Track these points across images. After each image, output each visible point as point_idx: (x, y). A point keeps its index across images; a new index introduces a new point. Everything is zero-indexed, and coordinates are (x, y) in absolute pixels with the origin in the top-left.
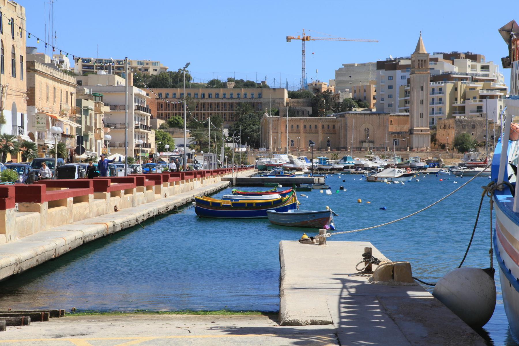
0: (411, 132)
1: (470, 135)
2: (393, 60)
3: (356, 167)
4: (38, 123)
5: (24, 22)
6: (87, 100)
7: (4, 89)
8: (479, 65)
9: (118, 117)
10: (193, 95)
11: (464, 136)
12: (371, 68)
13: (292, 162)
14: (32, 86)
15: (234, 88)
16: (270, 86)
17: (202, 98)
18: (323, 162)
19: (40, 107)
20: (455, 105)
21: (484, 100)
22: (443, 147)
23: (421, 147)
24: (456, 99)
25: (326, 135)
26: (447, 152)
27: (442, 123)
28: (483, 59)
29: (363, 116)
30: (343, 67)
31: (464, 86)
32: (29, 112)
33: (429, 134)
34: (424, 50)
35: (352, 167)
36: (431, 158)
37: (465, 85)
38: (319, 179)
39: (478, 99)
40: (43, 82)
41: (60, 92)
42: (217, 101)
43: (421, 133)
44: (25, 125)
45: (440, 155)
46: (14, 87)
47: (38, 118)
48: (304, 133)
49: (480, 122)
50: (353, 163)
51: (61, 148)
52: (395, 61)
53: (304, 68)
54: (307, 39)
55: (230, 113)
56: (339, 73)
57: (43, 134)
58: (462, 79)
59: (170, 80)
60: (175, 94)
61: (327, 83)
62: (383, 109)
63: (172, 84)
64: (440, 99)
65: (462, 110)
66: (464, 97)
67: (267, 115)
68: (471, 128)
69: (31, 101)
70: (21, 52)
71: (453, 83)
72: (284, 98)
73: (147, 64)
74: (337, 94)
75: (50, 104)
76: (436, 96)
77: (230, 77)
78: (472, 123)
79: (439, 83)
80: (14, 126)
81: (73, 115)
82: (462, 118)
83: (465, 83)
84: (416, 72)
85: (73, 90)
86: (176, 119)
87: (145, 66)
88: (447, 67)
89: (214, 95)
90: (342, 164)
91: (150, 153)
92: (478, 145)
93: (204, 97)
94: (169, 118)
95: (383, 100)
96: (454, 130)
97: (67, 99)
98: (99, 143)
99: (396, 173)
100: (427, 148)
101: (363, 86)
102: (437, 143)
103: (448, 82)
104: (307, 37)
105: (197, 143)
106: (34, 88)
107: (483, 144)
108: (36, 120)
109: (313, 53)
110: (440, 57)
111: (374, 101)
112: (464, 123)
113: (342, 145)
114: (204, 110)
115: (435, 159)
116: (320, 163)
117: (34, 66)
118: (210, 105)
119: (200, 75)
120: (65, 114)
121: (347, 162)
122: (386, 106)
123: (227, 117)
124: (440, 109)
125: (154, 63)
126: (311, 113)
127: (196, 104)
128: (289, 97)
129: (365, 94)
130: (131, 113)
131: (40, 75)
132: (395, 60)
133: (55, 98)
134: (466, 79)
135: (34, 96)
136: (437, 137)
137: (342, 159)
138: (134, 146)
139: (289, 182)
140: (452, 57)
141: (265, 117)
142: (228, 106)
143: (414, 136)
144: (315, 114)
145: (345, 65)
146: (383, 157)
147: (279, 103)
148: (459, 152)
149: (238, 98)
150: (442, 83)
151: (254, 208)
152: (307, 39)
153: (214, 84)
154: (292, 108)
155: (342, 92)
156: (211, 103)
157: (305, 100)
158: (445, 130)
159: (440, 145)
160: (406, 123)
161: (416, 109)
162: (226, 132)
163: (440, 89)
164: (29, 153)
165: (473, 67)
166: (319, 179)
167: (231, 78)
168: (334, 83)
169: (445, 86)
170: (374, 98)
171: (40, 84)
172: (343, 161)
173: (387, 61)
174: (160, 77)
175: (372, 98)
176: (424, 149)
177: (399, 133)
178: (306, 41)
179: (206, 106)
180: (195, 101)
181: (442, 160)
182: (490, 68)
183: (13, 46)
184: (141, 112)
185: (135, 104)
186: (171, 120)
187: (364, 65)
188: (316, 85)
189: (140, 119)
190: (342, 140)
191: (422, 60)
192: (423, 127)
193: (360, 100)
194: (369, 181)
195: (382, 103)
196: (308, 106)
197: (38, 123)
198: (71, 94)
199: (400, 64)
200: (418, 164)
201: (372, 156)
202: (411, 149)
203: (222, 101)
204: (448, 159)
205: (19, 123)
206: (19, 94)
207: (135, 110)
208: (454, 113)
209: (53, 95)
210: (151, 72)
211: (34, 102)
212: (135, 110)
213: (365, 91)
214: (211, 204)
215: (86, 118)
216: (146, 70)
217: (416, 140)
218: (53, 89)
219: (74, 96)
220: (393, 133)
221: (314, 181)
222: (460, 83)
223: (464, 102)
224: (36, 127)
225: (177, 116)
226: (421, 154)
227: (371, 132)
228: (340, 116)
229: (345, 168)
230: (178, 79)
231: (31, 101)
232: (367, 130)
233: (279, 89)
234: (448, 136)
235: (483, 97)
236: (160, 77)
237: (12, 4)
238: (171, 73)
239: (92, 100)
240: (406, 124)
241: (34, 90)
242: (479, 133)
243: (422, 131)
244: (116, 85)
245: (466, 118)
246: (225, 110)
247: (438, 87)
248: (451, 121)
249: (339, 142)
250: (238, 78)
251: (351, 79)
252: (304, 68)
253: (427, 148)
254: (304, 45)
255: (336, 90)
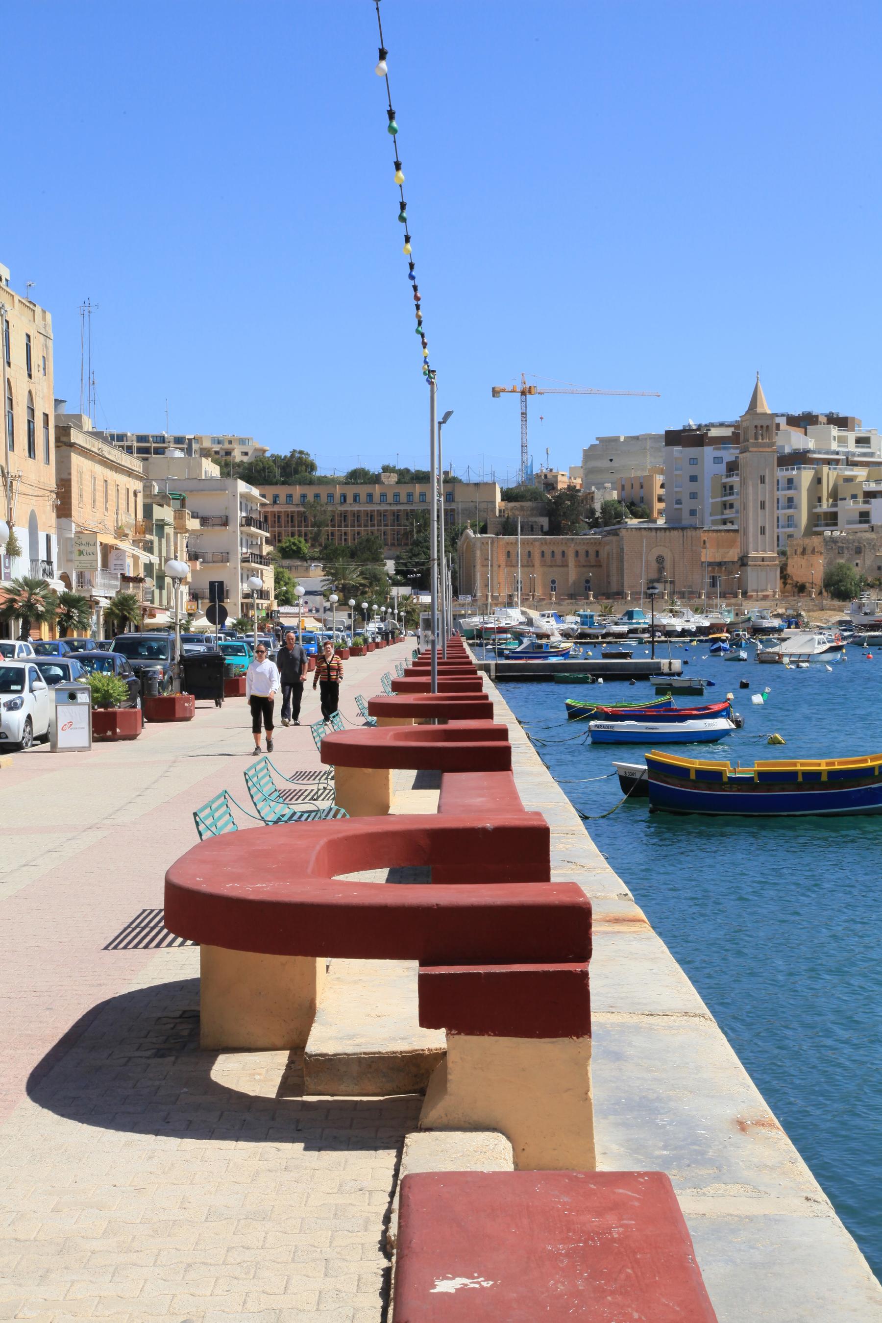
0: (743, 562)
1: (851, 566)
2: (694, 427)
3: (652, 629)
4: (81, 553)
5: (50, 344)
6: (162, 506)
7: (14, 482)
8: (851, 437)
9: (216, 539)
10: (324, 499)
11: (841, 567)
12: (649, 444)
13: (530, 622)
14: (65, 476)
15: (397, 483)
16: (464, 479)
17: (341, 504)
18: (586, 620)
19: (81, 521)
20: (818, 510)
21: (873, 501)
22: (801, 589)
23: (762, 591)
24: (820, 500)
25: (584, 569)
26: (813, 599)
27: (798, 545)
28: (859, 426)
29: (654, 533)
30: (598, 442)
31: (833, 475)
32: (60, 529)
33: (776, 565)
34: (766, 407)
35: (644, 631)
36: (784, 611)
37: (835, 473)
38: (670, 663)
39: (861, 499)
40: (84, 470)
41: (115, 489)
42: (369, 508)
43: (761, 563)
44: (54, 558)
45: (800, 604)
46: (32, 477)
47: (81, 544)
48: (576, 567)
49: (869, 541)
50: (645, 623)
51: (128, 606)
52: (699, 429)
53: (524, 446)
54: (530, 392)
55: (393, 530)
56: (590, 454)
57: (87, 576)
58: (828, 462)
59: (277, 471)
60: (290, 496)
61: (567, 474)
62: (680, 520)
63: (282, 479)
64: (790, 500)
65: (832, 519)
66: (835, 495)
67: (470, 532)
68: (853, 552)
69: (64, 510)
70: (44, 406)
71: (813, 468)
72: (495, 502)
73: (230, 442)
74: (589, 493)
75: (97, 515)
76: (783, 494)
77: (386, 463)
78: (856, 544)
79: (787, 470)
80: (34, 560)
81: (138, 537)
82: (836, 534)
83: (835, 469)
84: (751, 449)
85: (138, 485)
86: (294, 544)
87: (227, 446)
88: (796, 440)
89: (363, 498)
90: (624, 624)
91: (268, 608)
92: (868, 585)
93: (345, 501)
94: (280, 541)
95: (679, 502)
96: (823, 557)
97: (128, 504)
98: (182, 592)
99: (816, 645)
100: (775, 592)
101: (640, 477)
102: (789, 581)
103: (805, 468)
104: (530, 388)
105: (337, 587)
106: (69, 480)
107: (877, 583)
108: (77, 548)
109: (542, 418)
110: (782, 421)
111: (658, 506)
112: (840, 545)
113: (614, 588)
114: (346, 526)
115: (790, 612)
116: (583, 623)
117: (69, 435)
118: (357, 515)
119: (332, 463)
120: (126, 535)
121: (634, 621)
122: (686, 514)
123: (389, 537)
124: (790, 518)
125: (242, 441)
126: (546, 528)
127: (329, 514)
128: (503, 500)
129: (642, 493)
130: (235, 532)
131: (79, 454)
132: (699, 427)
133: (106, 502)
134: (837, 461)
135: (70, 497)
136: (790, 570)
137: (624, 615)
138: (240, 595)
139: (609, 670)
140: (805, 421)
141: (468, 536)
142: (390, 518)
143: (749, 568)
144: (555, 529)
145: (602, 440)
146: (697, 610)
147: (486, 510)
148: (832, 599)
149: (409, 502)
150: (793, 469)
151: (825, 786)
152: (530, 392)
153: (357, 476)
154: (510, 520)
155: (598, 489)
156: (359, 511)
157: (535, 505)
158: (805, 557)
159: (796, 586)
160: (731, 544)
161: (754, 519)
162: (390, 566)
163: (790, 481)
164: (72, 617)
165: (842, 440)
166: (670, 663)
167: (388, 466)
168: (581, 472)
169: (799, 475)
170: (660, 500)
171: (80, 473)
172: (625, 619)
173: (684, 431)
174: (257, 465)
175: (655, 499)
176: (769, 592)
177: (720, 564)
178: (528, 396)
179: (350, 518)
180: (330, 508)
181: (803, 613)
182: (872, 441)
183: (30, 392)
184: (252, 529)
185: (241, 514)
186: (284, 545)
187: (636, 438)
188: (546, 476)
189: (250, 543)
190: (614, 579)
191: (762, 427)
192: (765, 551)
193: (633, 504)
194: (762, 662)
195: (677, 509)
196: (542, 515)
197: (81, 553)
198: (135, 495)
199: (709, 435)
200: (766, 624)
201: (676, 608)
202: (745, 594)
203: (379, 508)
204: (814, 611)
205: (43, 556)
206: (42, 493)
207: (242, 525)
208: (817, 525)
209: (103, 495)
210: (237, 456)
211: (70, 509)
212: (242, 525)
213: (642, 487)
214: (693, 776)
215: (160, 541)
216: (228, 453)
217: (753, 577)
218: (103, 483)
219: (140, 496)
220: (710, 564)
221: (660, 669)
222: (825, 468)
223: (835, 505)
224: (77, 563)
225: (296, 537)
226: (763, 602)
227: (668, 564)
228: (609, 533)
229: (631, 631)
230: (293, 469)
231: (64, 510)
232: (660, 560)
233: (486, 484)
234: (813, 570)
235: (870, 495)
236: (257, 465)
237: (28, 304)
238: (276, 459)
239: (169, 505)
240: (731, 547)
241: (70, 486)
242: (868, 563)
243: (763, 559)
244: (204, 477)
245: (843, 534)
246: (386, 525)
247: (785, 476)
248: (816, 541)
249: (609, 583)
250: (401, 466)
251: (613, 464)
252: (524, 446)
253: (775, 592)
254: (524, 402)
255: (586, 484)
